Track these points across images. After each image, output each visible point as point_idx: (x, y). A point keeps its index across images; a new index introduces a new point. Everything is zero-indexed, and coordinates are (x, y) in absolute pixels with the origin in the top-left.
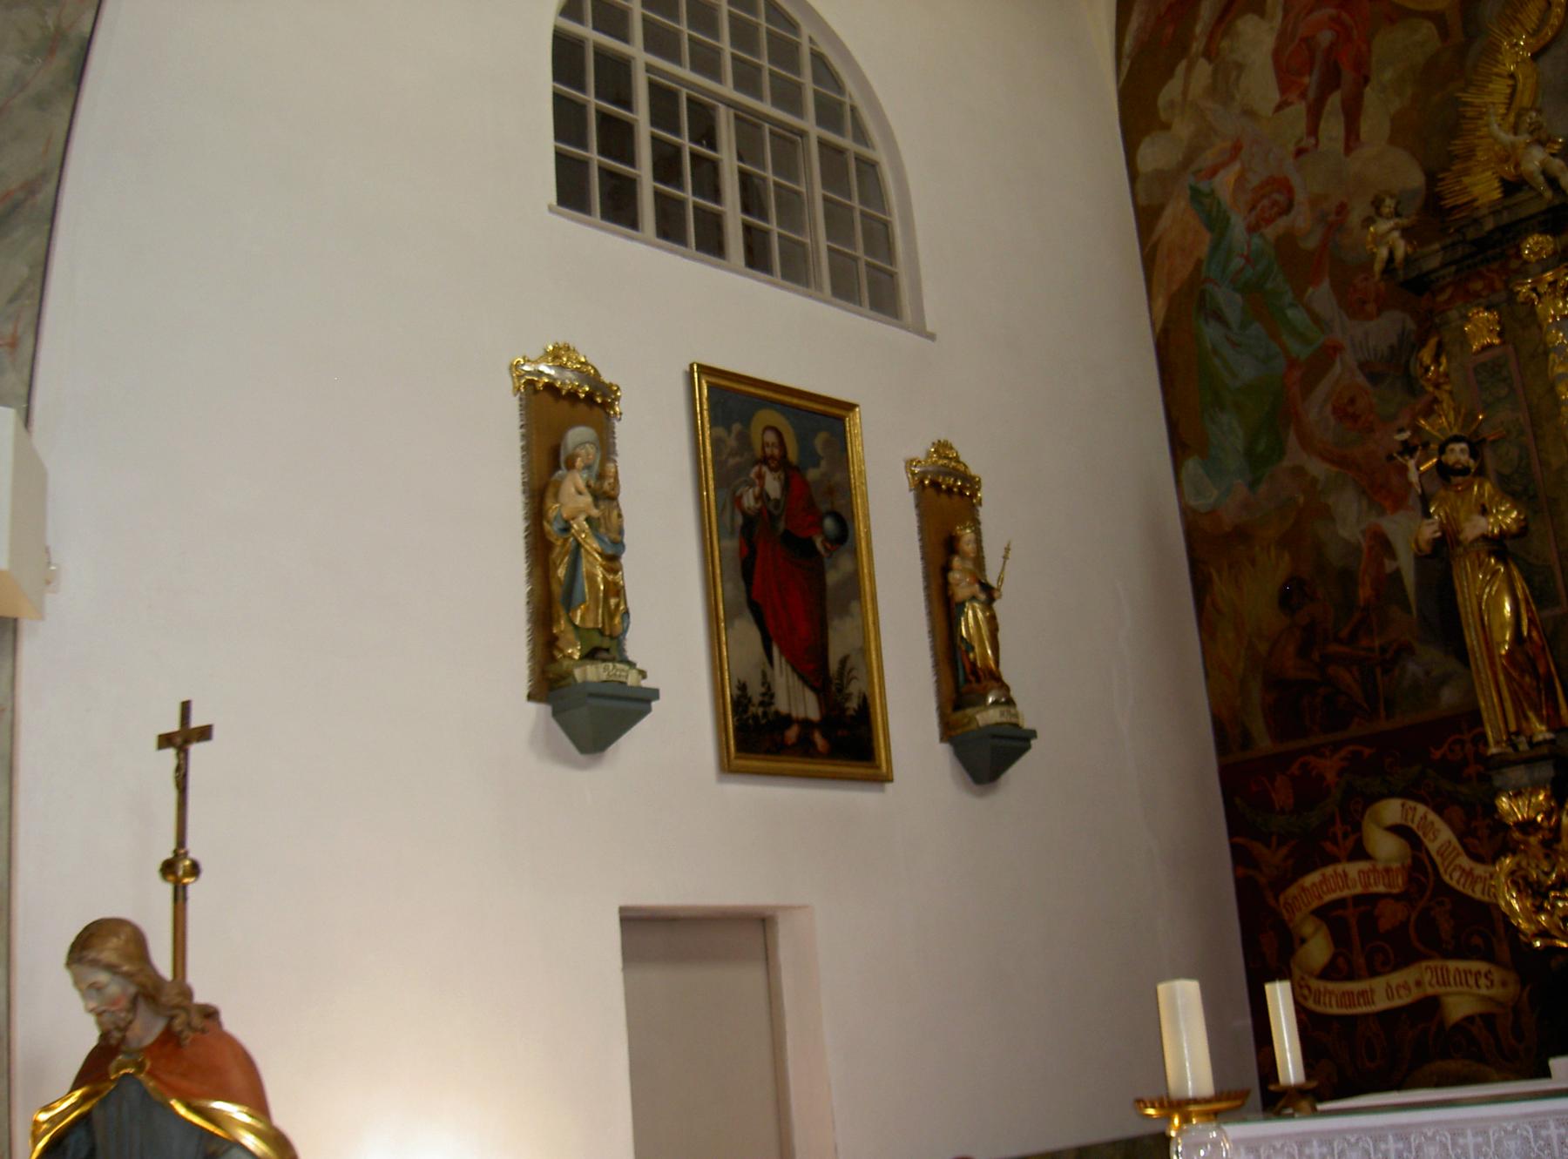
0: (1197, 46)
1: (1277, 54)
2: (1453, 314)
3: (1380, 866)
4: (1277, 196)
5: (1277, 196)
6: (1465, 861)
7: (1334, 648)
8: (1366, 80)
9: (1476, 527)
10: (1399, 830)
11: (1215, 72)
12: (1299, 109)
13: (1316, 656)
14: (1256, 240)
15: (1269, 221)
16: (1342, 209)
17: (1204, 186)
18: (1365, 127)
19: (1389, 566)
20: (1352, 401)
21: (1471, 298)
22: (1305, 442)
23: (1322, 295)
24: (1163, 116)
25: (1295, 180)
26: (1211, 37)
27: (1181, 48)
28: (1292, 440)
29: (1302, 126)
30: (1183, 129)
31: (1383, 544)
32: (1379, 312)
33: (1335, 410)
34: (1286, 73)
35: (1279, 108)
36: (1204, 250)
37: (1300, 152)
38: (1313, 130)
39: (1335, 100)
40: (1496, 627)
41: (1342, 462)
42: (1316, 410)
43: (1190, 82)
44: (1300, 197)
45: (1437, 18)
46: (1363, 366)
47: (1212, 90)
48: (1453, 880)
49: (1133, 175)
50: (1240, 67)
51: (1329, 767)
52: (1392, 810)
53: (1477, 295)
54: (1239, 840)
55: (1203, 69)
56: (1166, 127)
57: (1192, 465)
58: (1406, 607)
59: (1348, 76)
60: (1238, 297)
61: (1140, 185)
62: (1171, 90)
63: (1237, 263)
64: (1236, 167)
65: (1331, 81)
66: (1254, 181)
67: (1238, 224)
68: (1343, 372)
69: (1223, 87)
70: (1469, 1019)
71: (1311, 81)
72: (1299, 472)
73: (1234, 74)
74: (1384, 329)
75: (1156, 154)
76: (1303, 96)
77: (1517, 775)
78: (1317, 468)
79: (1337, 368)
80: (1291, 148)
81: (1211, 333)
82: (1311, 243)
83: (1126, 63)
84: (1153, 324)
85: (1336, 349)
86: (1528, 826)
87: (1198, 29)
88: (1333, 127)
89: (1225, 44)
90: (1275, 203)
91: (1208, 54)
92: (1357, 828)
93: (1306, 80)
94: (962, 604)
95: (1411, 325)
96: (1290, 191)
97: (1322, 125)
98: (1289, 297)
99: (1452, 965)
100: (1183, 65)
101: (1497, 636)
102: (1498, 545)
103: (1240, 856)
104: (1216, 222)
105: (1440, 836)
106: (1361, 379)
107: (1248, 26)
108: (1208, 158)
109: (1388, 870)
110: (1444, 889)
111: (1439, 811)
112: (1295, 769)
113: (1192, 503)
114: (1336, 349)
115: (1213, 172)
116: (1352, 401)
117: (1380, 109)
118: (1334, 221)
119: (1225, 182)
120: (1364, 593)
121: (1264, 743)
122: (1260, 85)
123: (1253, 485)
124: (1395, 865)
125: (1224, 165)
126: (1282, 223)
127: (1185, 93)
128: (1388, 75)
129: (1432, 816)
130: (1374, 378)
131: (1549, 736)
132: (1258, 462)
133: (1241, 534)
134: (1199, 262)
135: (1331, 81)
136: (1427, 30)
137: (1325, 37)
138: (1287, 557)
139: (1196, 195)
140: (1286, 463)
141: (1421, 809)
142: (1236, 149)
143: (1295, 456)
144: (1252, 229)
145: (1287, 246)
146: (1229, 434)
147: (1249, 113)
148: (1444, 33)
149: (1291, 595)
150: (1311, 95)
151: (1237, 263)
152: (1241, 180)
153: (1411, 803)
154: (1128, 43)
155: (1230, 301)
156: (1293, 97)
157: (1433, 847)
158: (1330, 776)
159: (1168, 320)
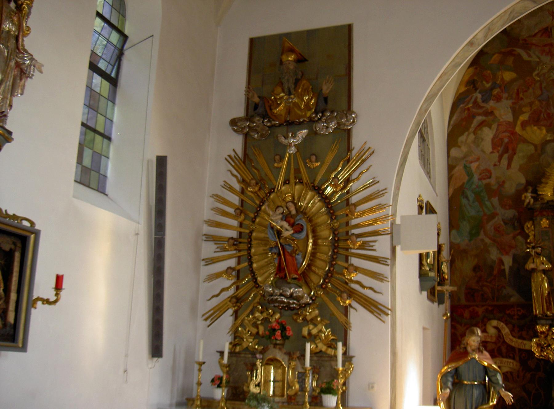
0: (472, 130)
1: (493, 140)
2: (538, 218)
3: (490, 335)
4: (487, 174)
5: (487, 174)
6: (511, 337)
7: (485, 283)
8: (515, 154)
9: (542, 267)
10: (496, 328)
11: (475, 138)
12: (496, 155)
13: (480, 284)
14: (480, 183)
15: (484, 179)
16: (504, 182)
17: (468, 165)
18: (513, 165)
19: (502, 267)
20: (499, 227)
21: (544, 216)
22: (486, 234)
23: (495, 200)
24: (459, 144)
25: (493, 171)
26: (476, 129)
27: (467, 129)
28: (482, 232)
29: (496, 159)
30: (464, 149)
31: (501, 262)
32: (509, 209)
33: (494, 228)
34: (495, 144)
35: (491, 153)
36: (466, 181)
37: (495, 165)
38: (499, 161)
39: (506, 156)
40: (544, 289)
41: (494, 241)
42: (489, 227)
43: (466, 138)
44: (493, 176)
45: (536, 146)
46: (503, 220)
47: (474, 142)
48: (508, 341)
49: (448, 156)
50: (482, 139)
51: (480, 310)
52: (495, 323)
53: (544, 215)
54: (453, 323)
55: (472, 136)
56: (459, 147)
57: (454, 232)
58: (506, 278)
59: (510, 151)
60: (473, 195)
61: (450, 159)
62: (462, 138)
63: (474, 186)
64: (477, 163)
65: (506, 151)
66: (482, 168)
67: (476, 177)
68: (498, 220)
69: (477, 141)
70: (507, 372)
71: (501, 149)
72: (482, 240)
73: (480, 140)
74: (510, 213)
75: (455, 152)
76: (498, 152)
77: (543, 322)
78: (487, 241)
79: (496, 219)
80: (493, 163)
81: (464, 201)
82: (495, 187)
83: (451, 127)
84: (448, 194)
85: (497, 214)
86: (543, 333)
87: (472, 126)
88: (505, 162)
89: (479, 132)
90: (486, 175)
91: (475, 133)
92: (485, 325)
93: (499, 148)
94: (442, 263)
95: (517, 214)
96: (491, 174)
97: (502, 161)
98: (487, 198)
99: (505, 360)
100: (466, 133)
101: (544, 292)
102: (544, 272)
103: (453, 327)
104: (470, 175)
105: (506, 331)
106: (502, 223)
107: (486, 130)
108: (470, 159)
109: (491, 336)
110: (504, 342)
111: (506, 324)
112: (471, 309)
113: (453, 241)
114: (497, 214)
115: (471, 162)
116: (499, 227)
117: (517, 162)
118: (502, 184)
119: (474, 166)
120: (495, 272)
121: (463, 302)
122: (487, 146)
123: (470, 240)
124: (493, 335)
125: (475, 161)
126: (488, 181)
127: (466, 140)
128: (521, 154)
129: (504, 326)
130: (506, 224)
131: (551, 315)
132: (473, 235)
133: (465, 251)
134: (464, 183)
135: (506, 151)
136: (532, 148)
137: (506, 140)
138: (476, 260)
139: (465, 167)
140: (480, 237)
141: (502, 324)
142: (478, 159)
143: (482, 236)
144: (480, 179)
145: (488, 186)
146: (466, 227)
147: (483, 151)
148: (536, 150)
149: (476, 269)
150: (500, 152)
151: (474, 186)
152: (478, 167)
153: (499, 322)
154: (452, 122)
155: (469, 193)
156: (495, 151)
157: (504, 332)
158: (480, 313)
159: (453, 194)
